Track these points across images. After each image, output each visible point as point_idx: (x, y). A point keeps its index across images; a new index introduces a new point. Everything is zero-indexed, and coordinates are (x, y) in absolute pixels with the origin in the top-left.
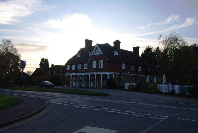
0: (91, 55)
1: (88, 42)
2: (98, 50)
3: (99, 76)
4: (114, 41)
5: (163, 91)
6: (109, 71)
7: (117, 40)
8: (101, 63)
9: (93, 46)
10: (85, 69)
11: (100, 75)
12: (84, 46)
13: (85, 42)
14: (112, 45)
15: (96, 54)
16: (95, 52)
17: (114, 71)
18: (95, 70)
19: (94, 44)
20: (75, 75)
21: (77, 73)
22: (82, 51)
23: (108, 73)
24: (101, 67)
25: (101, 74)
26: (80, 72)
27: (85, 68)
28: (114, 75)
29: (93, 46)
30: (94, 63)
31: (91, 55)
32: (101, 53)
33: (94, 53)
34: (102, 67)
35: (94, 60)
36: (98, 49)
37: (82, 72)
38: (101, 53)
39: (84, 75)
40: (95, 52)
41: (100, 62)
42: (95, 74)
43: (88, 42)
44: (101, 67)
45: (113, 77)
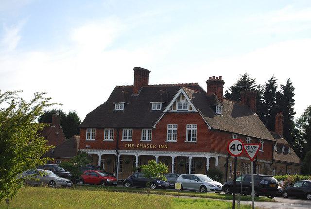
0: (166, 111)
5: (225, 163)
7: (217, 75)
8: (190, 131)
9: (149, 84)
10: (146, 143)
11: (186, 159)
12: (128, 80)
13: (133, 72)
14: (293, 98)
15: (177, 109)
16: (175, 104)
17: (219, 152)
18: (172, 147)
19: (153, 80)
21: (119, 151)
22: (119, 93)
23: (208, 156)
24: (189, 140)
25: (191, 156)
28: (217, 160)
29: (149, 84)
30: (172, 128)
31: (166, 111)
32: (191, 108)
35: (172, 122)
36: (183, 99)
37: (135, 149)
38: (191, 108)
40: (175, 104)
41: (188, 129)
42: (173, 155)
43: (141, 74)
44: (189, 140)
45: (217, 165)
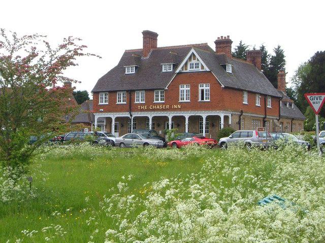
1: (150, 37)
2: (193, 62)
3: (195, 120)
4: (284, 54)
6: (223, 108)
7: (225, 35)
8: (202, 91)
9: (158, 46)
10: (159, 104)
15: (189, 70)
18: (185, 107)
20: (127, 118)
21: (133, 113)
22: (130, 57)
24: (202, 98)
26: (142, 110)
27: (100, 104)
29: (158, 46)
30: (185, 89)
33: (183, 68)
34: (205, 100)
35: (183, 83)
36: (194, 59)
37: (148, 110)
39: (117, 119)
40: (186, 64)
41: (200, 88)
43: (150, 37)
44: (202, 98)
